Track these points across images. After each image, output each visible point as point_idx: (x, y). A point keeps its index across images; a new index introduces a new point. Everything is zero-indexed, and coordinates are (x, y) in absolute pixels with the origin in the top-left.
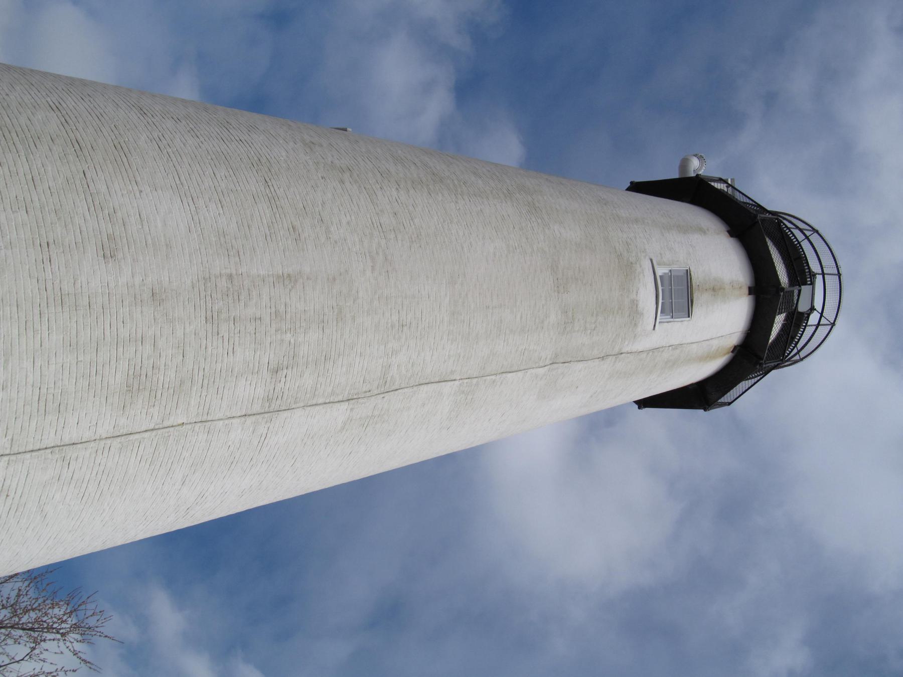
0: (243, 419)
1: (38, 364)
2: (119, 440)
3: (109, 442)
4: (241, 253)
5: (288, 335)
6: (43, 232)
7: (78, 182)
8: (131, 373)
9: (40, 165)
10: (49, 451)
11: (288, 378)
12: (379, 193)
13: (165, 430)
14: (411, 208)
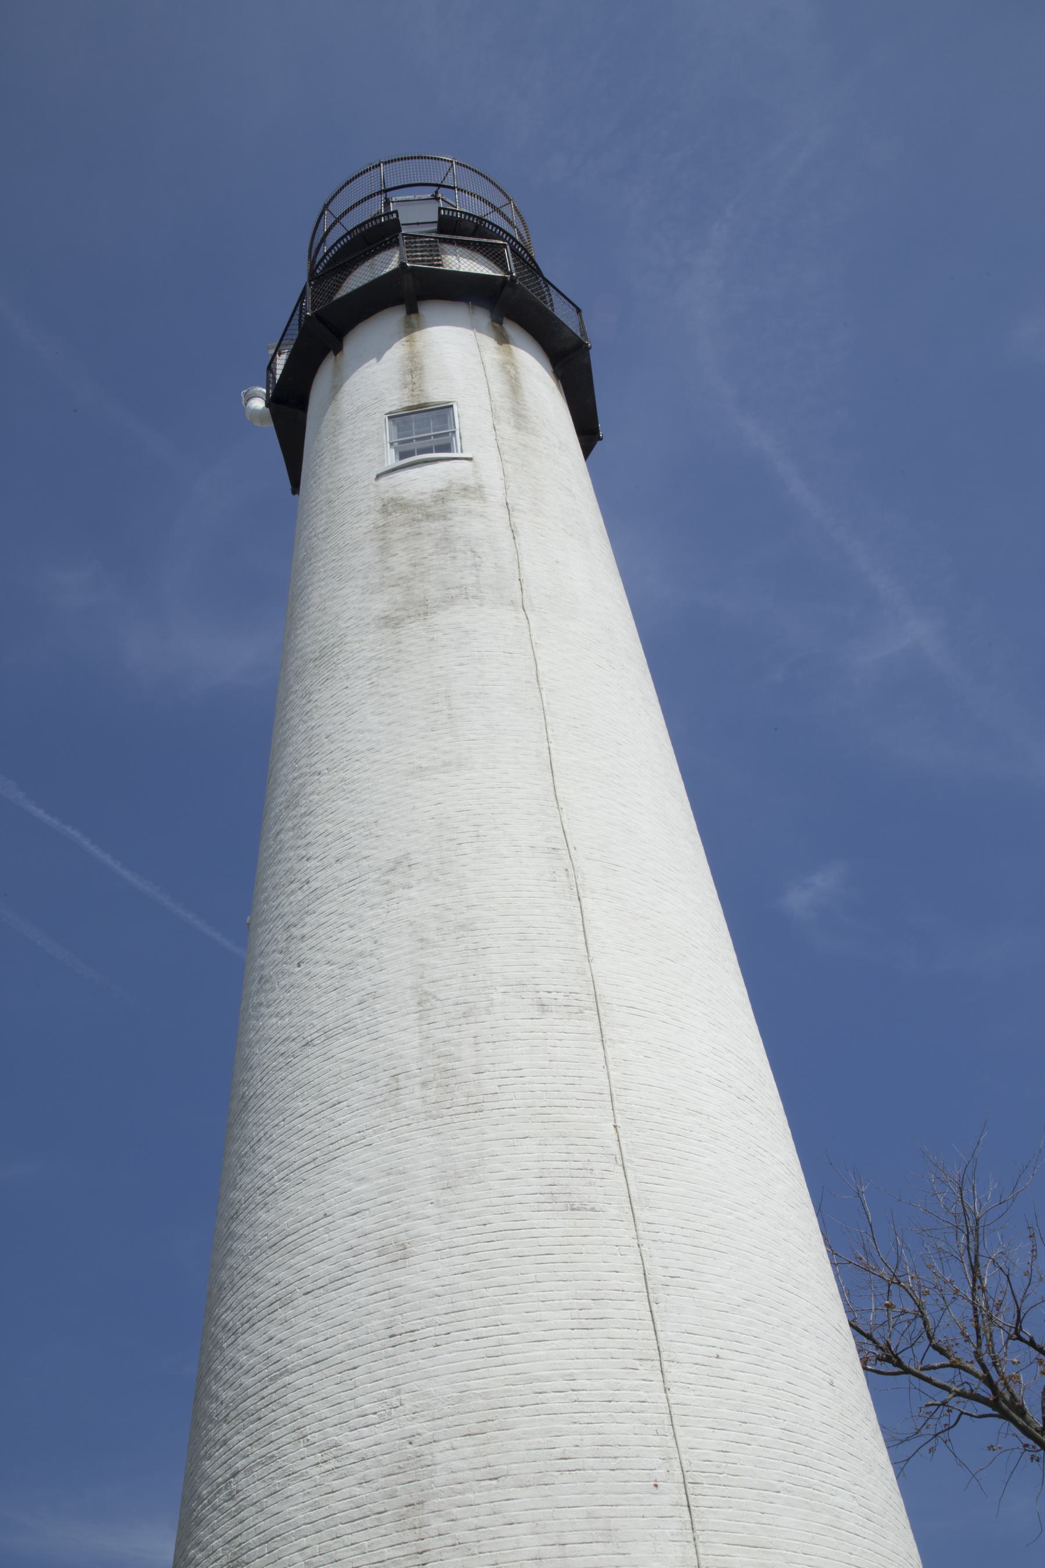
0: (607, 1044)
1: (541, 1335)
2: (637, 1213)
3: (640, 1226)
4: (394, 1072)
5: (494, 996)
6: (377, 1345)
7: (317, 1301)
8: (549, 1206)
9: (299, 1355)
10: (654, 1307)
11: (552, 988)
12: (314, 885)
13: (623, 1150)
14: (329, 839)
